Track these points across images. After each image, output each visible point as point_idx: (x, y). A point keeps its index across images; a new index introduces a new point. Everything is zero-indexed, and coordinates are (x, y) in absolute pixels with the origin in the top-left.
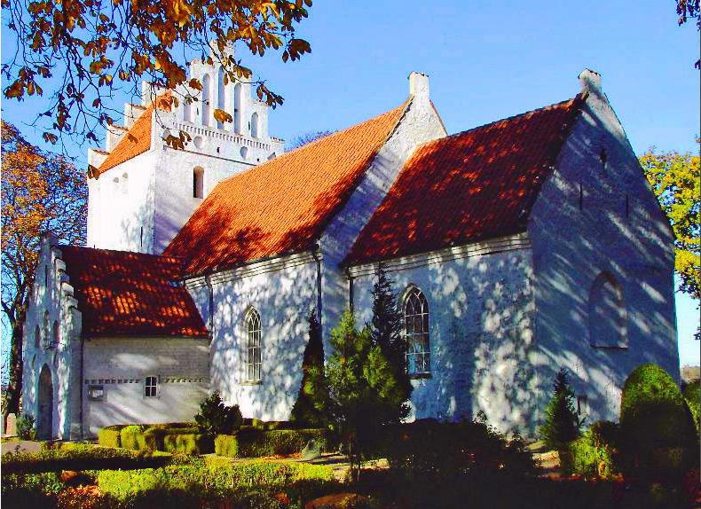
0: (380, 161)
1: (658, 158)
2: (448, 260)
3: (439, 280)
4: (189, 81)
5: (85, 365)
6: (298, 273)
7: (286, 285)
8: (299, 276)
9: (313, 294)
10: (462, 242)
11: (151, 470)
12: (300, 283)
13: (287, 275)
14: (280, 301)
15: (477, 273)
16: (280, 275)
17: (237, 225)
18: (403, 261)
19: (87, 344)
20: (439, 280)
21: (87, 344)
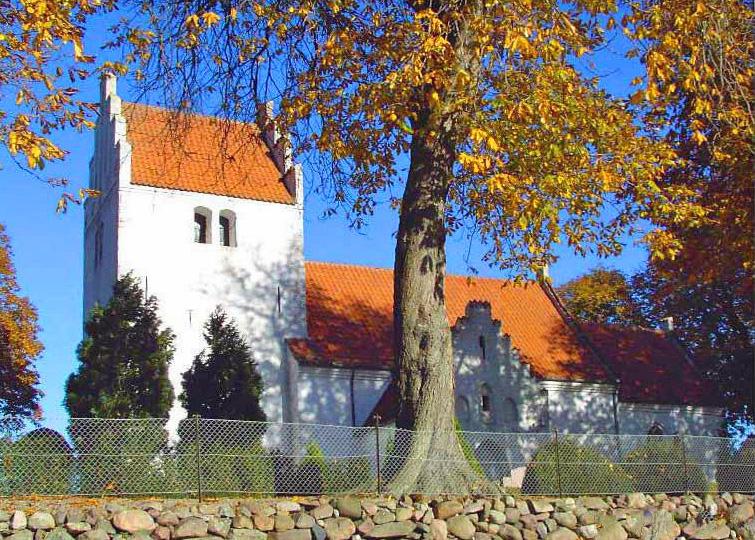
0: (561, 367)
1: (426, 360)
2: (683, 413)
3: (676, 424)
4: (547, 356)
5: (350, 407)
6: (592, 399)
7: (580, 405)
8: (593, 400)
9: (609, 417)
10: (696, 405)
11: (261, 404)
12: (594, 407)
13: (581, 398)
14: (573, 416)
15: (697, 424)
16: (574, 396)
17: (172, 333)
18: (656, 407)
19: (381, 298)
20: (676, 424)
21: (381, 298)
